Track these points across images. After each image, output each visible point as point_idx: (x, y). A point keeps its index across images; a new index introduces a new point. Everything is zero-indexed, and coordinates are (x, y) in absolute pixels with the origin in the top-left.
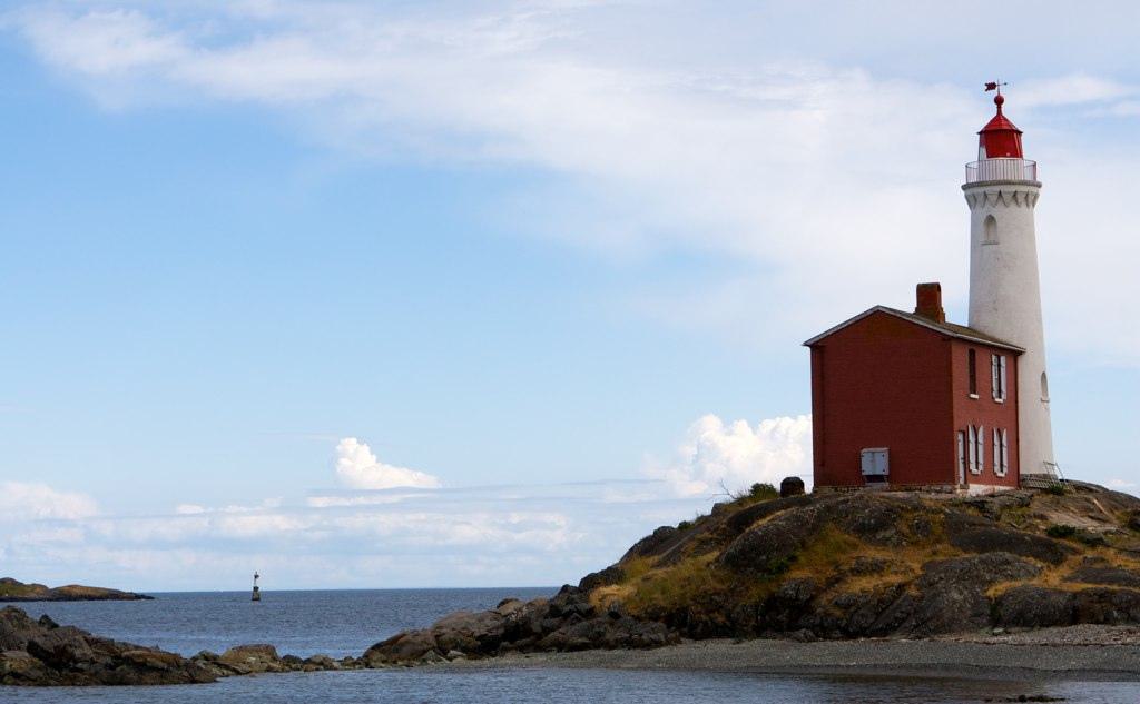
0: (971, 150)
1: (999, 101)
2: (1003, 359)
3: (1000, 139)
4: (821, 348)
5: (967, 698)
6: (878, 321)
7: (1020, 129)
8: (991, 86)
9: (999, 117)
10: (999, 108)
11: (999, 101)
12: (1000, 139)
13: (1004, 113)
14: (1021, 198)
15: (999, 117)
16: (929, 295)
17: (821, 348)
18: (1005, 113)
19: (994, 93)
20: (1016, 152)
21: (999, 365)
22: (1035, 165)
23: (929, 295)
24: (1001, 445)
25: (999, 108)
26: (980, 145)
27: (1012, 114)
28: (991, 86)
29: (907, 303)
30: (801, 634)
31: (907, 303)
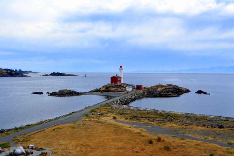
3: (121, 67)
12: (121, 67)
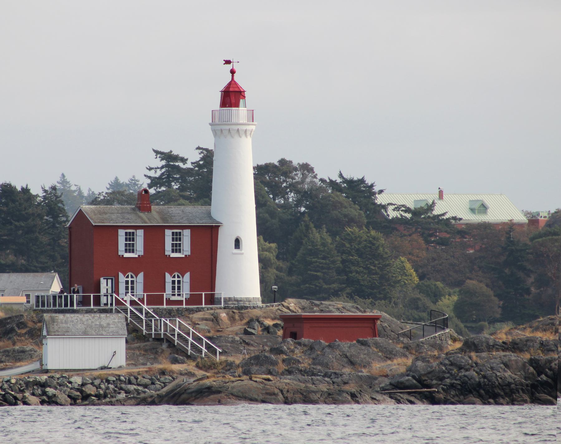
1: (233, 72)
3: (231, 96)
9: (232, 83)
10: (233, 76)
11: (233, 72)
14: (248, 133)
15: (232, 83)
18: (236, 79)
19: (229, 67)
25: (233, 76)
28: (228, 62)
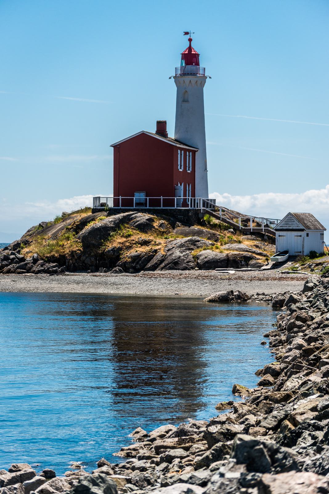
0: (178, 63)
1: (190, 40)
2: (183, 152)
3: (191, 58)
4: (119, 149)
5: (239, 310)
6: (142, 138)
7: (199, 53)
8: (187, 33)
10: (190, 43)
11: (190, 40)
12: (191, 58)
13: (192, 46)
16: (161, 126)
17: (119, 149)
19: (188, 37)
20: (197, 64)
21: (181, 155)
22: (205, 69)
23: (161, 126)
24: (189, 190)
25: (190, 43)
26: (182, 59)
27: (197, 48)
28: (187, 33)
29: (152, 130)
30: (117, 268)
31: (152, 130)
